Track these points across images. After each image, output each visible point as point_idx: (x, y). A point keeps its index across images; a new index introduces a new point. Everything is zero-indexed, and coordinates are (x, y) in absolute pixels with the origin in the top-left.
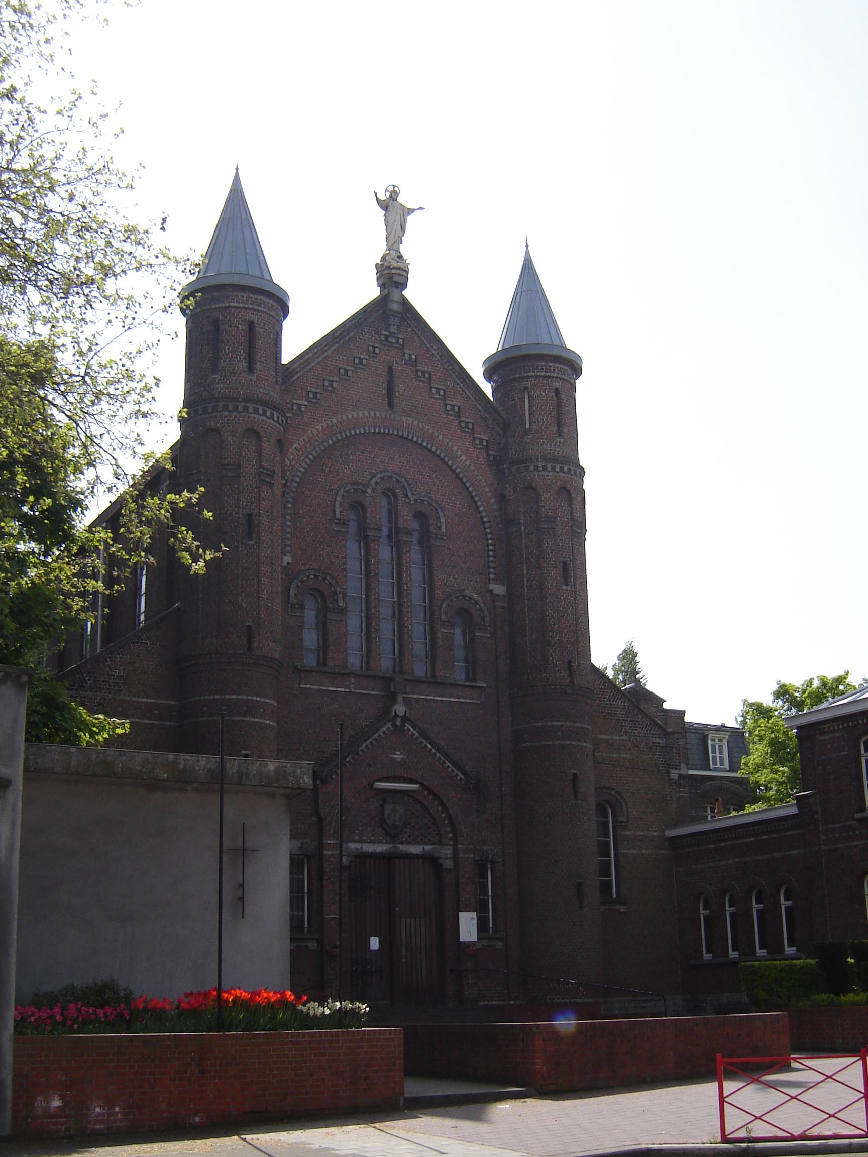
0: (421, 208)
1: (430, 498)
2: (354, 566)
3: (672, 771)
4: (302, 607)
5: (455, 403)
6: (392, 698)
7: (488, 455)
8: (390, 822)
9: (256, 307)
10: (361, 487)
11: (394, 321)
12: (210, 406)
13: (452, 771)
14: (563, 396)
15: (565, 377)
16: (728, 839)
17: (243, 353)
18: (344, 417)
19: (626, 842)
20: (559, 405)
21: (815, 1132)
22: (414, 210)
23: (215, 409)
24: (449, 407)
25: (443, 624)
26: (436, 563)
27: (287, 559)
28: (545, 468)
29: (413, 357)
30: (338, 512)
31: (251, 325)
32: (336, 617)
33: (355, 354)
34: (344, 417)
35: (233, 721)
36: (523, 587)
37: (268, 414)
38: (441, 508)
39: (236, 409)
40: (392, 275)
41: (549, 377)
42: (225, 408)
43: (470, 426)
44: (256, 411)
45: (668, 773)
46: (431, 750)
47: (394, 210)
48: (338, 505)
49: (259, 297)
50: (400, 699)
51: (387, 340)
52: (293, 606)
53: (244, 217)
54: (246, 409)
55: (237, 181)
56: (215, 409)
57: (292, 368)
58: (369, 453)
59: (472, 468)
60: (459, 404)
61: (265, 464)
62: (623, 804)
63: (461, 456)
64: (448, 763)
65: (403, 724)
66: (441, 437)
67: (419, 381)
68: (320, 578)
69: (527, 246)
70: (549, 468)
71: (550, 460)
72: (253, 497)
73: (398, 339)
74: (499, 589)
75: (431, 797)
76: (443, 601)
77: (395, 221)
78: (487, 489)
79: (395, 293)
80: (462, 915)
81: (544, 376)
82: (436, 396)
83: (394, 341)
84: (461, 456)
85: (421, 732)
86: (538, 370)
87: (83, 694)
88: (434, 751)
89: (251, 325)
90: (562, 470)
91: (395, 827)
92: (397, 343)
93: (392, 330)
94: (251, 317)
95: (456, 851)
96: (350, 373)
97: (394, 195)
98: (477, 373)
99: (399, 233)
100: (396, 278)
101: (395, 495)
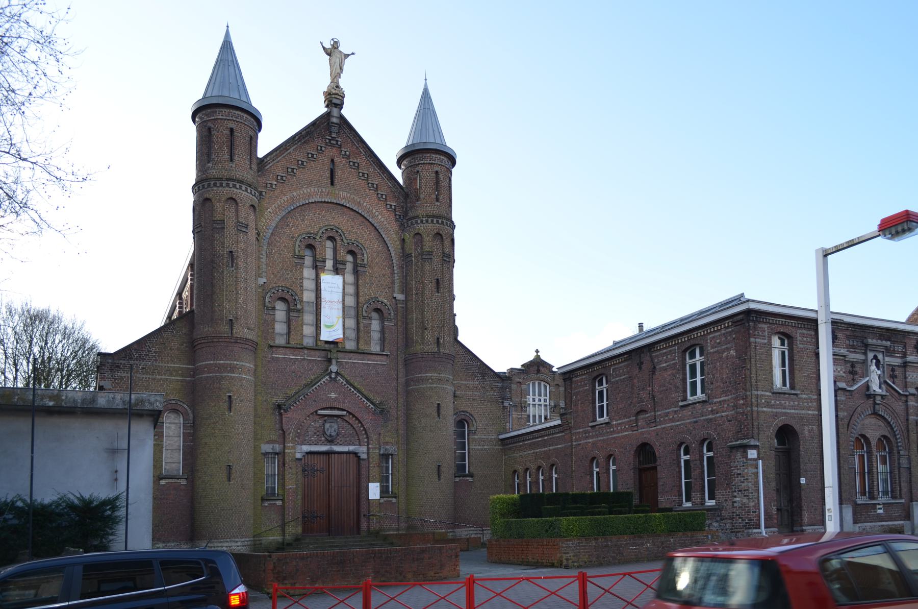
0: (353, 54)
2: (309, 284)
4: (274, 309)
6: (329, 361)
11: (335, 129)
12: (206, 184)
17: (226, 149)
20: (437, 182)
21: (617, 578)
22: (348, 55)
23: (209, 186)
25: (364, 318)
26: (360, 281)
27: (262, 281)
28: (427, 221)
31: (232, 130)
32: (295, 314)
39: (221, 185)
40: (334, 99)
42: (215, 185)
44: (234, 186)
47: (334, 52)
49: (237, 112)
50: (334, 362)
52: (268, 309)
54: (228, 185)
55: (227, 34)
56: (209, 186)
61: (241, 220)
71: (430, 216)
74: (400, 297)
78: (394, 236)
79: (335, 112)
85: (347, 381)
86: (430, 160)
87: (132, 362)
90: (438, 222)
91: (331, 436)
95: (368, 449)
97: (335, 45)
98: (390, 162)
99: (339, 71)
100: (335, 101)
101: (335, 240)
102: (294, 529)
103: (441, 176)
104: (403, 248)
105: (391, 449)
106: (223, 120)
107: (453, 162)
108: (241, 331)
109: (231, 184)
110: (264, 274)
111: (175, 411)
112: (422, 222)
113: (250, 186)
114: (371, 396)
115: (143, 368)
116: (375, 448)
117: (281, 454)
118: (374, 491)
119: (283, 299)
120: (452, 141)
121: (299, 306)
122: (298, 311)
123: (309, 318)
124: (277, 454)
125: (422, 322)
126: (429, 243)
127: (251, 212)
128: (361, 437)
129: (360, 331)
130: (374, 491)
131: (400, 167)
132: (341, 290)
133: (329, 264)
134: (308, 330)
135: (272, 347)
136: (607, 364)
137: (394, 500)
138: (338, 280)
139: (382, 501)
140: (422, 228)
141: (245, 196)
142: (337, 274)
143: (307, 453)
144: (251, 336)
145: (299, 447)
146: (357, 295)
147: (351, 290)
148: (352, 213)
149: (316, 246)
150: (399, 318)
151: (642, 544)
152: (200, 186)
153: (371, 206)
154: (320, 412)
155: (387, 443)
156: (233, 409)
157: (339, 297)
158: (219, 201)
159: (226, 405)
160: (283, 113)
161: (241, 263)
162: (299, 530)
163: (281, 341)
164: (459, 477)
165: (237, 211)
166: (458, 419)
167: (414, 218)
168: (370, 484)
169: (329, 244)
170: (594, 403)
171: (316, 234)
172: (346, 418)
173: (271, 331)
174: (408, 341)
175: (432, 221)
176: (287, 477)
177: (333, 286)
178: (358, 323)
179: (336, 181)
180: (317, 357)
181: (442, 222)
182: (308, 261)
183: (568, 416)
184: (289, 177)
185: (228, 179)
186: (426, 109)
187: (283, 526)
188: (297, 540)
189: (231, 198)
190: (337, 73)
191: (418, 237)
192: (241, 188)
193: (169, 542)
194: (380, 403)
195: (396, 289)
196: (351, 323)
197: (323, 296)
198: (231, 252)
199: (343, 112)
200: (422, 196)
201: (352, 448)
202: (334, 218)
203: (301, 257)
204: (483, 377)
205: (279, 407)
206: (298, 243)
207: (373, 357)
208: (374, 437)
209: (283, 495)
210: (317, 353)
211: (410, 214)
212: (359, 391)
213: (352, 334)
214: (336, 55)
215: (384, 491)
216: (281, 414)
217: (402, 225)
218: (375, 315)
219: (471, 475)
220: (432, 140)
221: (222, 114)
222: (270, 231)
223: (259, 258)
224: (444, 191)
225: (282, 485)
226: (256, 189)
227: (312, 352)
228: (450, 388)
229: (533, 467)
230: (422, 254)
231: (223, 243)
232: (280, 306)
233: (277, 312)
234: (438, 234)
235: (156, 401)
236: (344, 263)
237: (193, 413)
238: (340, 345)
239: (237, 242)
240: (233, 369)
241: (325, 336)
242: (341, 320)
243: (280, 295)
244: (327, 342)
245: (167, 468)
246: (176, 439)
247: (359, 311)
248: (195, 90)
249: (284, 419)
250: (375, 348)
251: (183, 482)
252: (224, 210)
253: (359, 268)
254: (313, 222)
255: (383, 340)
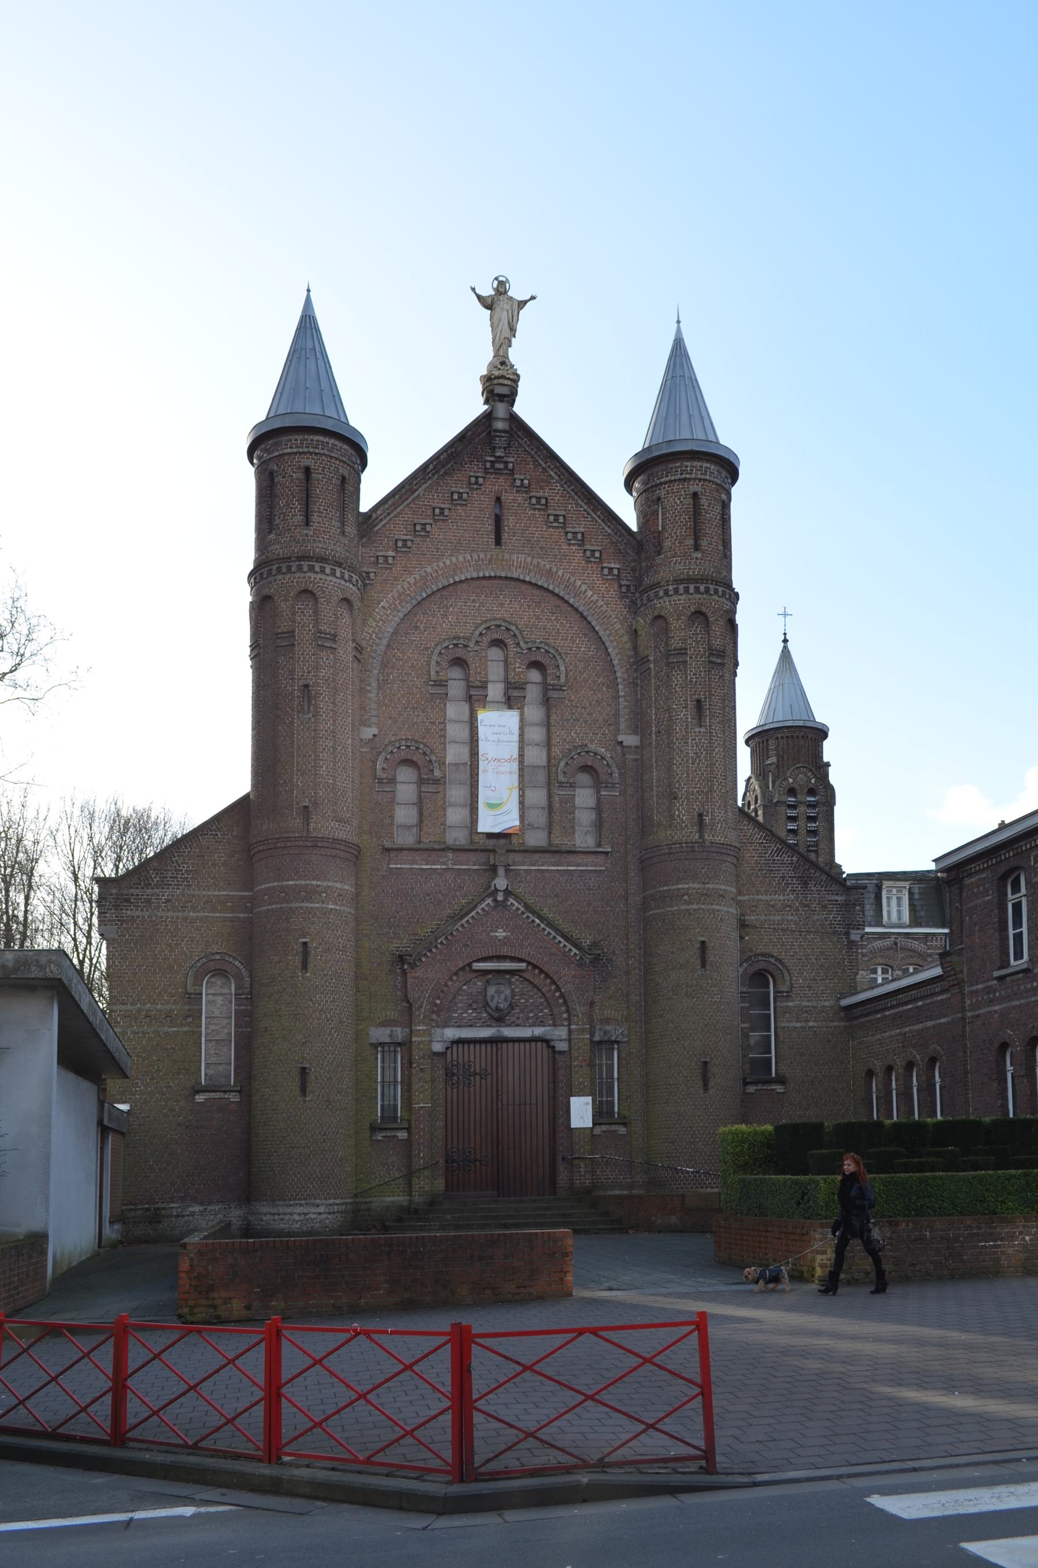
0: (533, 298)
1: (547, 644)
3: (852, 931)
4: (393, 781)
5: (577, 530)
6: (493, 870)
7: (620, 586)
8: (493, 1005)
9: (312, 450)
10: (461, 641)
13: (565, 946)
14: (702, 502)
15: (708, 477)
16: (892, 1007)
18: (441, 564)
19: (787, 1016)
22: (525, 302)
24: (570, 536)
25: (561, 785)
26: (553, 717)
27: (368, 733)
29: (526, 482)
30: (433, 673)
32: (431, 788)
33: (453, 489)
34: (441, 564)
35: (291, 908)
36: (650, 734)
37: (338, 574)
38: (560, 654)
40: (501, 386)
41: (685, 480)
43: (597, 554)
44: (311, 569)
45: (847, 934)
46: (538, 925)
47: (501, 305)
48: (433, 663)
50: (501, 871)
51: (493, 466)
52: (381, 781)
53: (318, 349)
54: (300, 568)
55: (308, 303)
56: (270, 574)
57: (374, 516)
58: (474, 601)
59: (600, 603)
60: (582, 530)
62: (785, 972)
63: (586, 591)
64: (559, 938)
65: (506, 899)
66: (560, 573)
67: (534, 509)
68: (395, 750)
69: (678, 322)
70: (681, 591)
72: (310, 665)
73: (506, 463)
74: (631, 740)
75: (542, 976)
76: (561, 760)
77: (500, 320)
78: (618, 626)
80: (574, 1100)
81: (680, 480)
82: (556, 524)
83: (501, 466)
84: (586, 591)
85: (527, 906)
86: (686, 472)
87: (149, 891)
88: (542, 926)
89: (307, 470)
91: (497, 1009)
92: (506, 468)
93: (498, 454)
94: (306, 462)
95: (570, 1031)
96: (446, 512)
97: (501, 287)
99: (507, 333)
100: (499, 390)
101: (505, 645)
102: (429, 1184)
103: (704, 501)
104: (635, 648)
105: (616, 1031)
106: (301, 452)
107: (733, 474)
108: (324, 826)
109: (305, 565)
110: (374, 720)
111: (220, 972)
112: (666, 593)
113: (340, 565)
114: (575, 934)
115: (167, 901)
116: (583, 1031)
117: (406, 1045)
118: (581, 1112)
119: (408, 762)
120: (730, 433)
121: (437, 773)
122: (437, 782)
123: (457, 793)
124: (399, 1044)
125: (670, 785)
126: (679, 632)
127: (343, 611)
128: (556, 1011)
129: (557, 812)
130: (581, 1112)
131: (631, 494)
132: (516, 737)
133: (495, 691)
134: (456, 816)
135: (388, 850)
136: (1024, 846)
137: (622, 1130)
138: (510, 719)
139: (598, 1130)
140: (666, 605)
141: (331, 583)
142: (510, 707)
143: (453, 1042)
144: (344, 832)
145: (439, 1031)
146: (549, 744)
147: (537, 734)
148: (536, 592)
149: (470, 660)
150: (629, 781)
151: (1012, 1237)
152: (259, 575)
153: (573, 574)
154: (478, 966)
155: (608, 1021)
156: (310, 966)
157: (512, 750)
158: (286, 600)
159: (298, 960)
160: (402, 424)
161: (324, 705)
162: (440, 1184)
163: (407, 839)
164: (755, 1083)
165: (316, 612)
166: (752, 970)
167: (652, 587)
168: (572, 1099)
169: (495, 653)
170: (1004, 928)
171: (469, 639)
172: (527, 975)
173: (387, 821)
174: (645, 824)
175: (687, 591)
176: (415, 1086)
177: (499, 731)
178: (550, 796)
179: (505, 536)
180: (471, 864)
181: (707, 590)
182: (456, 688)
183: (954, 958)
184: (418, 540)
185: (300, 559)
186: (679, 376)
187: (409, 1177)
188: (433, 1203)
189: (306, 591)
190: (503, 342)
191: (659, 623)
192: (323, 571)
193: (210, 1203)
194: (595, 944)
195: (622, 727)
196: (537, 796)
197: (481, 752)
198: (306, 686)
199: (519, 408)
200: (667, 544)
201: (538, 1031)
202: (502, 605)
203: (441, 684)
204: (805, 884)
205: (401, 959)
206: (435, 658)
207: (579, 858)
208: (580, 1009)
209: (409, 1121)
210: (472, 856)
211: (647, 581)
212: (549, 924)
213: (539, 818)
214: (502, 305)
215: (601, 1113)
216: (404, 972)
217: (634, 602)
218: (584, 778)
219: (781, 1080)
220: (686, 435)
221: (289, 445)
222: (385, 642)
223: (363, 691)
224: (711, 529)
225: (408, 1101)
226: (352, 569)
227: (463, 856)
228: (728, 910)
229: (900, 1063)
230: (668, 654)
231: (292, 672)
232: (405, 775)
233: (400, 787)
234: (699, 613)
235: (50, 962)
236: (521, 687)
237: (251, 977)
238: (514, 840)
239: (317, 668)
240: (310, 894)
241: (488, 823)
242: (516, 793)
243: (403, 755)
244: (490, 836)
245: (210, 1072)
246: (224, 1022)
247: (549, 776)
248: (255, 406)
249: (410, 981)
250: (584, 840)
251: (234, 1098)
252: (294, 614)
253: (551, 694)
254: (462, 617)
255: (599, 824)
